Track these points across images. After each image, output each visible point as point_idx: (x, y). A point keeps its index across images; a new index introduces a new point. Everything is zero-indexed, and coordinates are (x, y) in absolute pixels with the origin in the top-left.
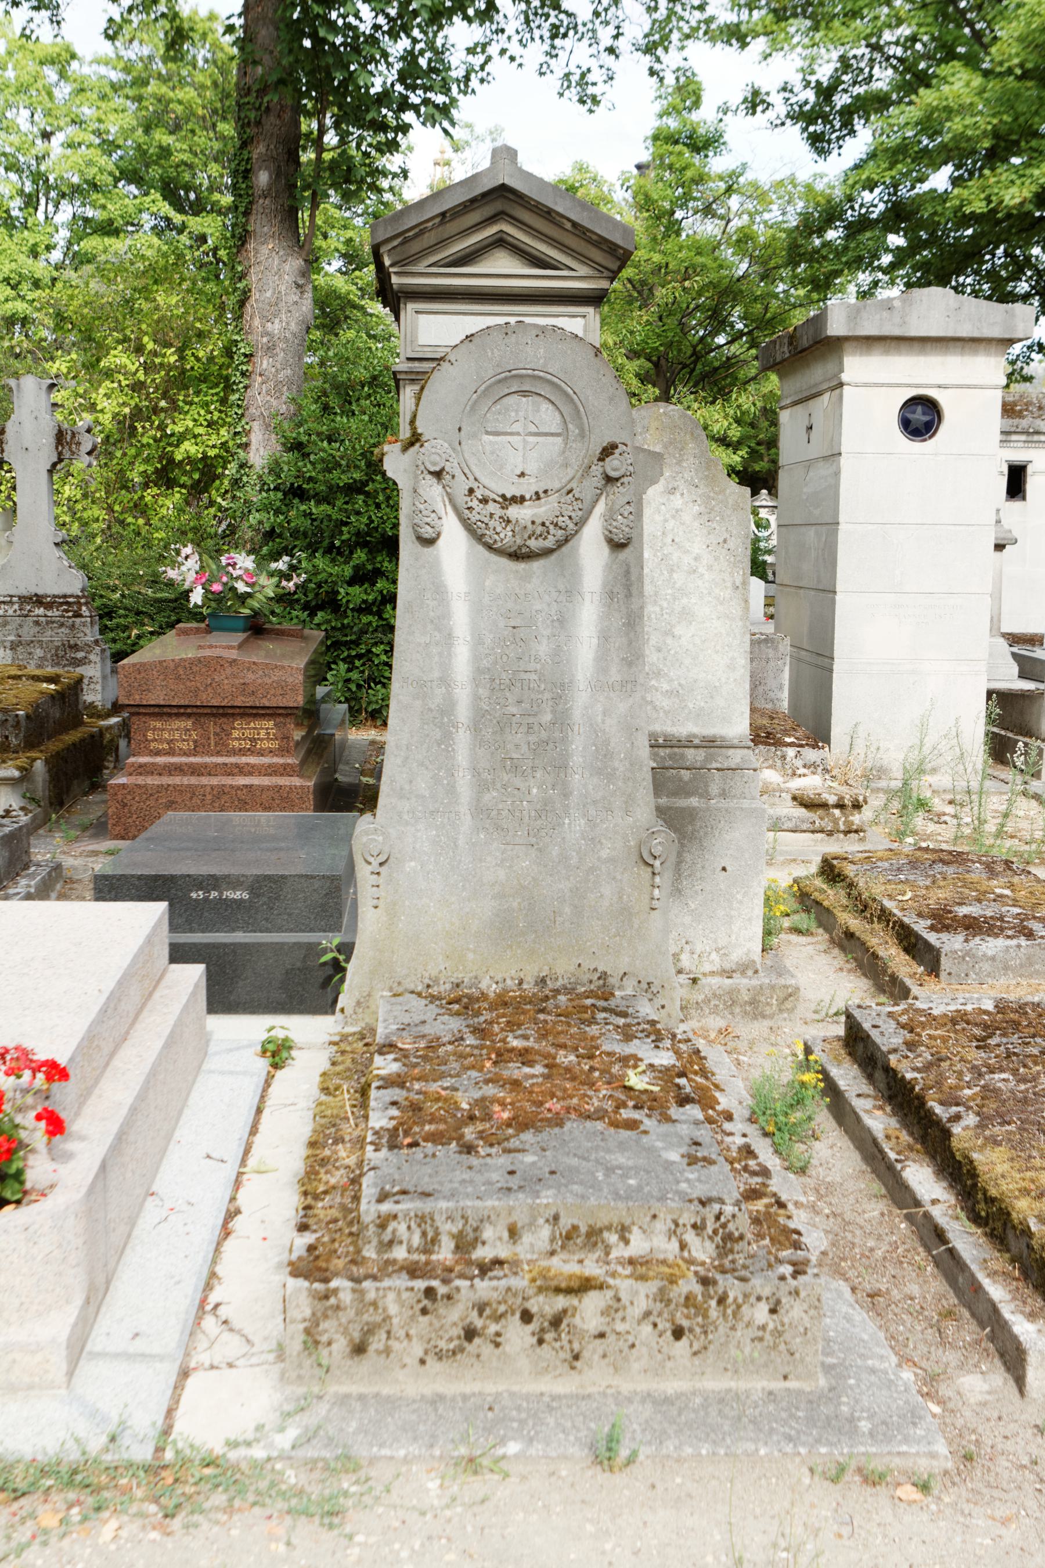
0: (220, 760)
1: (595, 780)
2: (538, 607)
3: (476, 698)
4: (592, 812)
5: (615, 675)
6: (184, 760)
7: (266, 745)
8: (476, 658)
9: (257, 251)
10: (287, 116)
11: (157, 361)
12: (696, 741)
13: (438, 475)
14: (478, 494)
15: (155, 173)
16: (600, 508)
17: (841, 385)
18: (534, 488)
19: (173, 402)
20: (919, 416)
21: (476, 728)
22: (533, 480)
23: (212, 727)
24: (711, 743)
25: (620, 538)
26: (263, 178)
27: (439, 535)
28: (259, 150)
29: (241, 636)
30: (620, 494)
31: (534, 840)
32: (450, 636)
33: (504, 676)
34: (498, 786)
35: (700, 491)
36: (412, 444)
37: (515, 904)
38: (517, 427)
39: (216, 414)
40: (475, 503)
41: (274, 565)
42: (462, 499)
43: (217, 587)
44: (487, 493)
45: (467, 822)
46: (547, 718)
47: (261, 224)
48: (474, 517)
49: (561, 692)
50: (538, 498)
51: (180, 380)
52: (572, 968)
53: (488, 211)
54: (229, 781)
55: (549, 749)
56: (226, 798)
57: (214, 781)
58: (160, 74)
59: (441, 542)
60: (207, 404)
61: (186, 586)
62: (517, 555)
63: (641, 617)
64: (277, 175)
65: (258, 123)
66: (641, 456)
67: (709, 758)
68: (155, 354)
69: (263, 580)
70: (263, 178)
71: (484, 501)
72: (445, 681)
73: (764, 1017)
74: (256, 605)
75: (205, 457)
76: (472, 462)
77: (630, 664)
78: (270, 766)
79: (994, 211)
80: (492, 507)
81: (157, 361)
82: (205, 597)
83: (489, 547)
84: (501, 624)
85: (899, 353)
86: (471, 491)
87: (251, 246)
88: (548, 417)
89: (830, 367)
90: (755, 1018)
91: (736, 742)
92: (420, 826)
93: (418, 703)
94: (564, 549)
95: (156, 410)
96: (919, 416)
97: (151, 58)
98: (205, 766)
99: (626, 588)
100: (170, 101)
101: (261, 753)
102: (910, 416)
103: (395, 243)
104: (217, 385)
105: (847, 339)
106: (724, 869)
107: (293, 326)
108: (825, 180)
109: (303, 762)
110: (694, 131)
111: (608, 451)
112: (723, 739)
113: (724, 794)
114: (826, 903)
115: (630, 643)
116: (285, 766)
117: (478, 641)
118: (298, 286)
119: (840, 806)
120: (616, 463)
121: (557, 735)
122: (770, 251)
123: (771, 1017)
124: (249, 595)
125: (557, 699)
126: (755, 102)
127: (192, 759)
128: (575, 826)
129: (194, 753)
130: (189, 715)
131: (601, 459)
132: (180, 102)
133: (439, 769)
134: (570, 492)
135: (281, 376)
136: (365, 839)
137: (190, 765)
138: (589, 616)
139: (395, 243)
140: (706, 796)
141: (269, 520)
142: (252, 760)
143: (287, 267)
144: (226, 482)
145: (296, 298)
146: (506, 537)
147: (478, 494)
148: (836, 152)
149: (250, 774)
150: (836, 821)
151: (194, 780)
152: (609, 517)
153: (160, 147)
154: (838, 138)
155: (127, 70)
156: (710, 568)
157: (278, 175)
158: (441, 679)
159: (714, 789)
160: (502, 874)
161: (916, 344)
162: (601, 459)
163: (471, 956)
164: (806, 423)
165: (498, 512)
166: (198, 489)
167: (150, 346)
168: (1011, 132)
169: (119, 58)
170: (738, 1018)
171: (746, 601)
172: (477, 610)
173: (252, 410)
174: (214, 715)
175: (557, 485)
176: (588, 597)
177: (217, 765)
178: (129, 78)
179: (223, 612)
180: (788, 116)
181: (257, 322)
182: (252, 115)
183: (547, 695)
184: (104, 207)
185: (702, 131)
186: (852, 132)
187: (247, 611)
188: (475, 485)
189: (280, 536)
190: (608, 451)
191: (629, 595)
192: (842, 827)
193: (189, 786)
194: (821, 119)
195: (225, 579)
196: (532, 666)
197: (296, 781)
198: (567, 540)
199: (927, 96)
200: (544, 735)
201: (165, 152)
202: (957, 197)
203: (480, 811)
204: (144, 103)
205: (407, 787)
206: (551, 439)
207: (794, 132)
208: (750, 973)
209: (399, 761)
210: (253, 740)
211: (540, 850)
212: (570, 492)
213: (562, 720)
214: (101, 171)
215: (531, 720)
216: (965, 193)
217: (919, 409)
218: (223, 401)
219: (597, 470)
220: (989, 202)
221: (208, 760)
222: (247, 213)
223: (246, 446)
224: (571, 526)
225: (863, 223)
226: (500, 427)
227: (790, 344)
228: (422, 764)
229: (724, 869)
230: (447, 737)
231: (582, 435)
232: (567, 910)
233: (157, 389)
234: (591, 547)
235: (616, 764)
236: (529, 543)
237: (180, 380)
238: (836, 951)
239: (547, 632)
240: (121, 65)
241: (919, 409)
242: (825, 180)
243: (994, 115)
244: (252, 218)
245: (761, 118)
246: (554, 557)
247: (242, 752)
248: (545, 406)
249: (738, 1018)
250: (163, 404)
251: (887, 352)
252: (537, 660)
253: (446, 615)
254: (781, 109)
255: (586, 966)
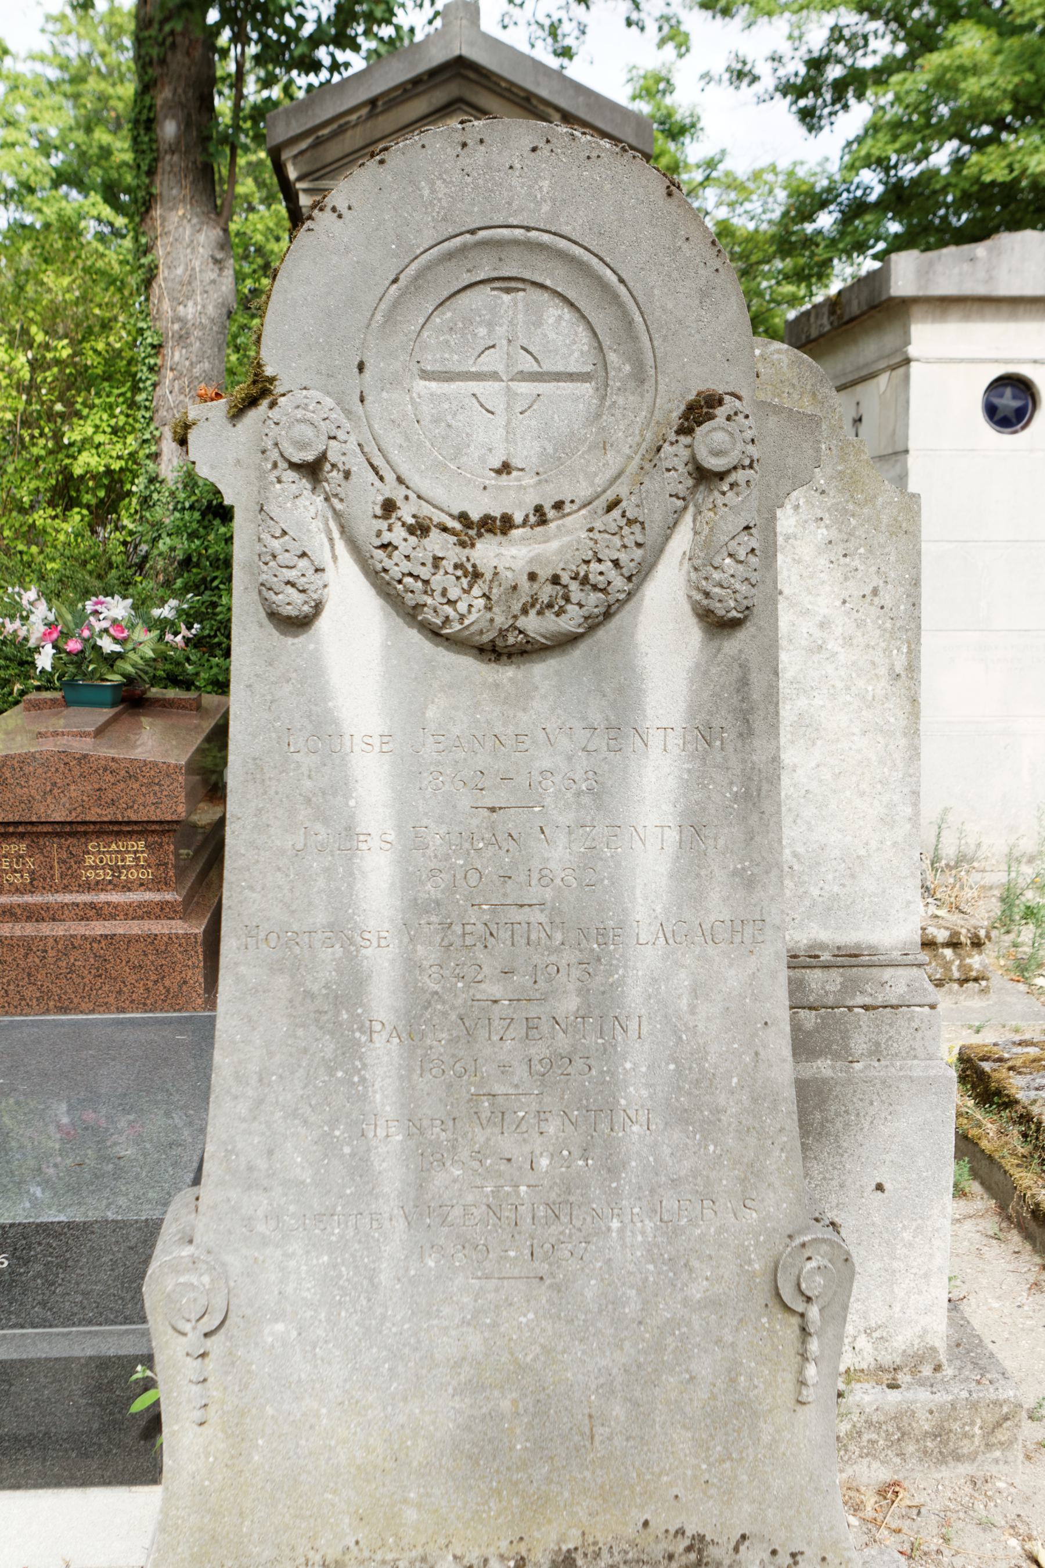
0: (68, 898)
1: (677, 1135)
2: (547, 764)
3: (411, 966)
4: (670, 1203)
5: (717, 907)
6: (16, 899)
7: (134, 875)
8: (409, 879)
9: (164, 219)
10: (198, 53)
11: (49, 356)
12: (826, 957)
13: (312, 470)
14: (406, 513)
15: (96, 175)
16: (682, 540)
17: (907, 361)
18: (532, 499)
19: (69, 404)
20: (1008, 401)
21: (412, 1031)
22: (529, 480)
23: (55, 850)
24: (850, 958)
25: (727, 607)
26: (169, 129)
27: (318, 607)
28: (164, 95)
29: (106, 713)
30: (729, 509)
31: (544, 1268)
32: (349, 831)
33: (472, 916)
34: (464, 1154)
35: (829, 501)
36: (252, 402)
37: (506, 1405)
38: (492, 361)
39: (122, 420)
40: (398, 535)
41: (156, 612)
42: (368, 526)
43: (74, 645)
44: (426, 510)
45: (395, 1238)
46: (569, 1004)
47: (166, 185)
48: (397, 565)
49: (594, 940)
50: (543, 521)
51: (77, 381)
52: (631, 1531)
53: (439, 96)
54: (80, 929)
55: (575, 1072)
56: (76, 953)
57: (59, 930)
58: (99, 71)
59: (323, 623)
60: (111, 407)
61: (32, 644)
62: (494, 651)
63: (774, 780)
64: (187, 124)
65: (163, 62)
66: (772, 422)
67: (851, 987)
68: (47, 347)
69: (140, 634)
70: (169, 129)
71: (420, 529)
72: (343, 931)
73: (958, 1458)
74: (130, 669)
75: (109, 472)
76: (392, 441)
77: (750, 883)
78: (140, 905)
79: (1017, 180)
80: (437, 543)
81: (49, 356)
82: (56, 658)
83: (434, 633)
84: (465, 801)
85: (983, 318)
86: (389, 507)
87: (157, 212)
88: (559, 335)
89: (889, 340)
90: (942, 1460)
91: (896, 955)
92: (295, 1247)
93: (281, 981)
94: (601, 634)
95: (51, 416)
96: (1008, 401)
97: (89, 55)
98: (47, 907)
99: (740, 715)
100: (109, 98)
101: (127, 887)
102: (996, 401)
103: (303, 145)
104: (123, 384)
105: (915, 300)
106: (880, 1187)
107: (211, 310)
108: (806, 167)
109: (188, 901)
110: (669, 115)
111: (700, 411)
112: (873, 951)
113: (876, 1052)
114: (984, 1144)
115: (750, 837)
116: (162, 905)
117: (411, 841)
118: (216, 261)
119: (954, 944)
120: (719, 437)
121: (593, 1041)
122: (750, 246)
123: (972, 1457)
124: (120, 656)
125: (590, 963)
126: (742, 75)
127: (28, 899)
128: (629, 1235)
129: (31, 888)
130: (22, 836)
131: (684, 430)
132: (120, 98)
133: (333, 1123)
134: (611, 507)
135: (197, 371)
136: (170, 1284)
137: (25, 907)
138: (657, 780)
139: (303, 145)
140: (844, 1055)
141: (182, 545)
142: (115, 897)
143: (202, 238)
144: (134, 500)
145: (213, 276)
146: (471, 611)
147: (406, 513)
148: (827, 129)
149: (113, 917)
150: (947, 966)
151: (29, 929)
152: (701, 562)
153: (101, 147)
154: (831, 114)
155: (62, 67)
156: (848, 641)
157: (188, 125)
158: (331, 927)
159: (859, 1044)
160: (475, 1341)
161: (1005, 308)
162: (684, 430)
163: (411, 1515)
164: (853, 414)
165: (453, 554)
166: (103, 512)
167: (40, 337)
168: (1031, 95)
169: (56, 53)
170: (912, 1462)
171: (914, 701)
172: (409, 773)
173: (163, 413)
174: (58, 835)
175: (583, 491)
176: (655, 739)
177: (64, 906)
178: (67, 77)
179: (79, 678)
180: (777, 89)
181: (166, 305)
182: (155, 52)
183: (569, 956)
184: (39, 210)
185: (678, 117)
186: (846, 107)
187: (116, 678)
188: (398, 494)
189: (197, 565)
190: (700, 411)
191: (747, 733)
192: (956, 975)
193: (22, 938)
194: (813, 92)
195: (86, 634)
196: (535, 893)
197: (178, 927)
198: (607, 615)
199: (935, 59)
200: (563, 1042)
201: (106, 152)
202: (977, 163)
203: (423, 1210)
204: (83, 100)
205: (262, 1164)
206: (567, 388)
207: (783, 105)
208: (927, 1370)
209: (243, 1108)
210: (116, 869)
211: (557, 1288)
212: (611, 507)
213: (602, 1010)
214: (36, 171)
215: (534, 1011)
216: (984, 160)
217: (1008, 392)
218: (132, 404)
219: (675, 454)
220: (1012, 171)
221: (50, 898)
222: (151, 172)
223: (155, 456)
224: (619, 583)
225: (858, 208)
226: (454, 362)
227: (832, 312)
228: (295, 1114)
229: (880, 1187)
230: (350, 1052)
231: (639, 377)
232: (618, 1410)
233: (51, 391)
234: (661, 625)
235: (722, 1100)
236: (522, 622)
237: (77, 381)
238: (1015, 1237)
239: (566, 819)
240: (58, 61)
241: (1008, 392)
242: (806, 167)
243: (1015, 74)
244: (158, 179)
245: (747, 92)
246: (578, 653)
247: (98, 886)
248: (554, 312)
249: (912, 1462)
250: (59, 407)
251: (967, 318)
252: (545, 878)
253: (340, 786)
254: (768, 82)
255: (658, 1525)
